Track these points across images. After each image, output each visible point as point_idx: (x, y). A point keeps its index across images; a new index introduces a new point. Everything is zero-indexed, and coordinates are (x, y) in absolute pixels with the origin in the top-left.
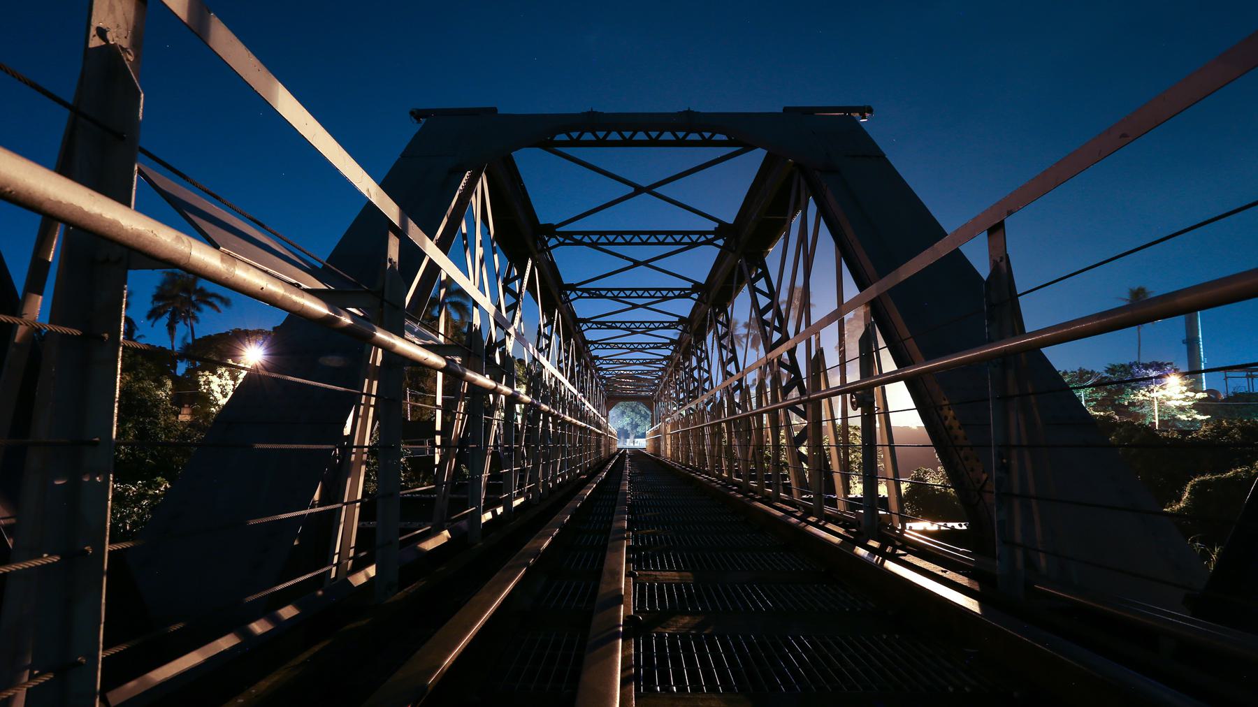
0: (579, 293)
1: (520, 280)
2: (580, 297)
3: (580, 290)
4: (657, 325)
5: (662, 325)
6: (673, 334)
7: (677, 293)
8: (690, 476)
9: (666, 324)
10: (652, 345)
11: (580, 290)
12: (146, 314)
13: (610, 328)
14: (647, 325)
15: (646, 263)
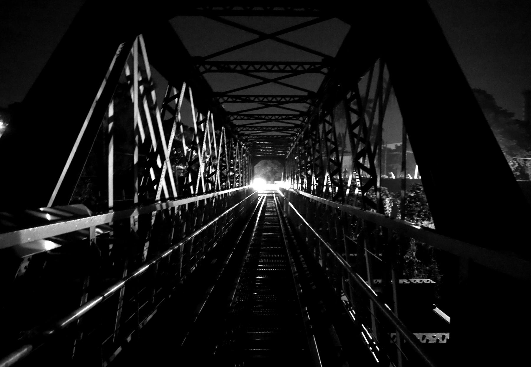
0: (208, 67)
1: (204, 123)
2: (226, 101)
3: (209, 63)
4: (288, 99)
5: (292, 100)
6: (303, 107)
7: (306, 67)
8: (101, 123)
9: (296, 99)
10: (284, 117)
11: (209, 63)
12: (283, 187)
13: (243, 101)
14: (279, 99)
15: (273, 36)
